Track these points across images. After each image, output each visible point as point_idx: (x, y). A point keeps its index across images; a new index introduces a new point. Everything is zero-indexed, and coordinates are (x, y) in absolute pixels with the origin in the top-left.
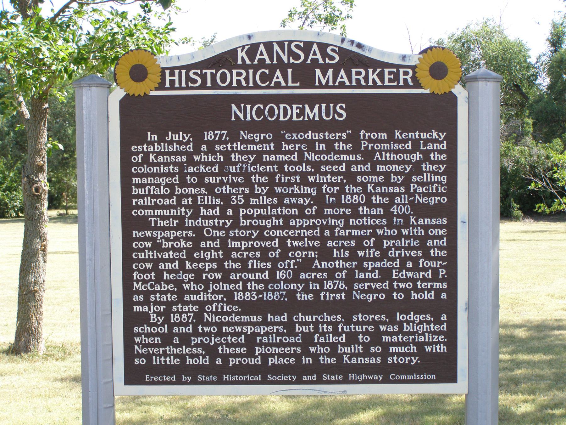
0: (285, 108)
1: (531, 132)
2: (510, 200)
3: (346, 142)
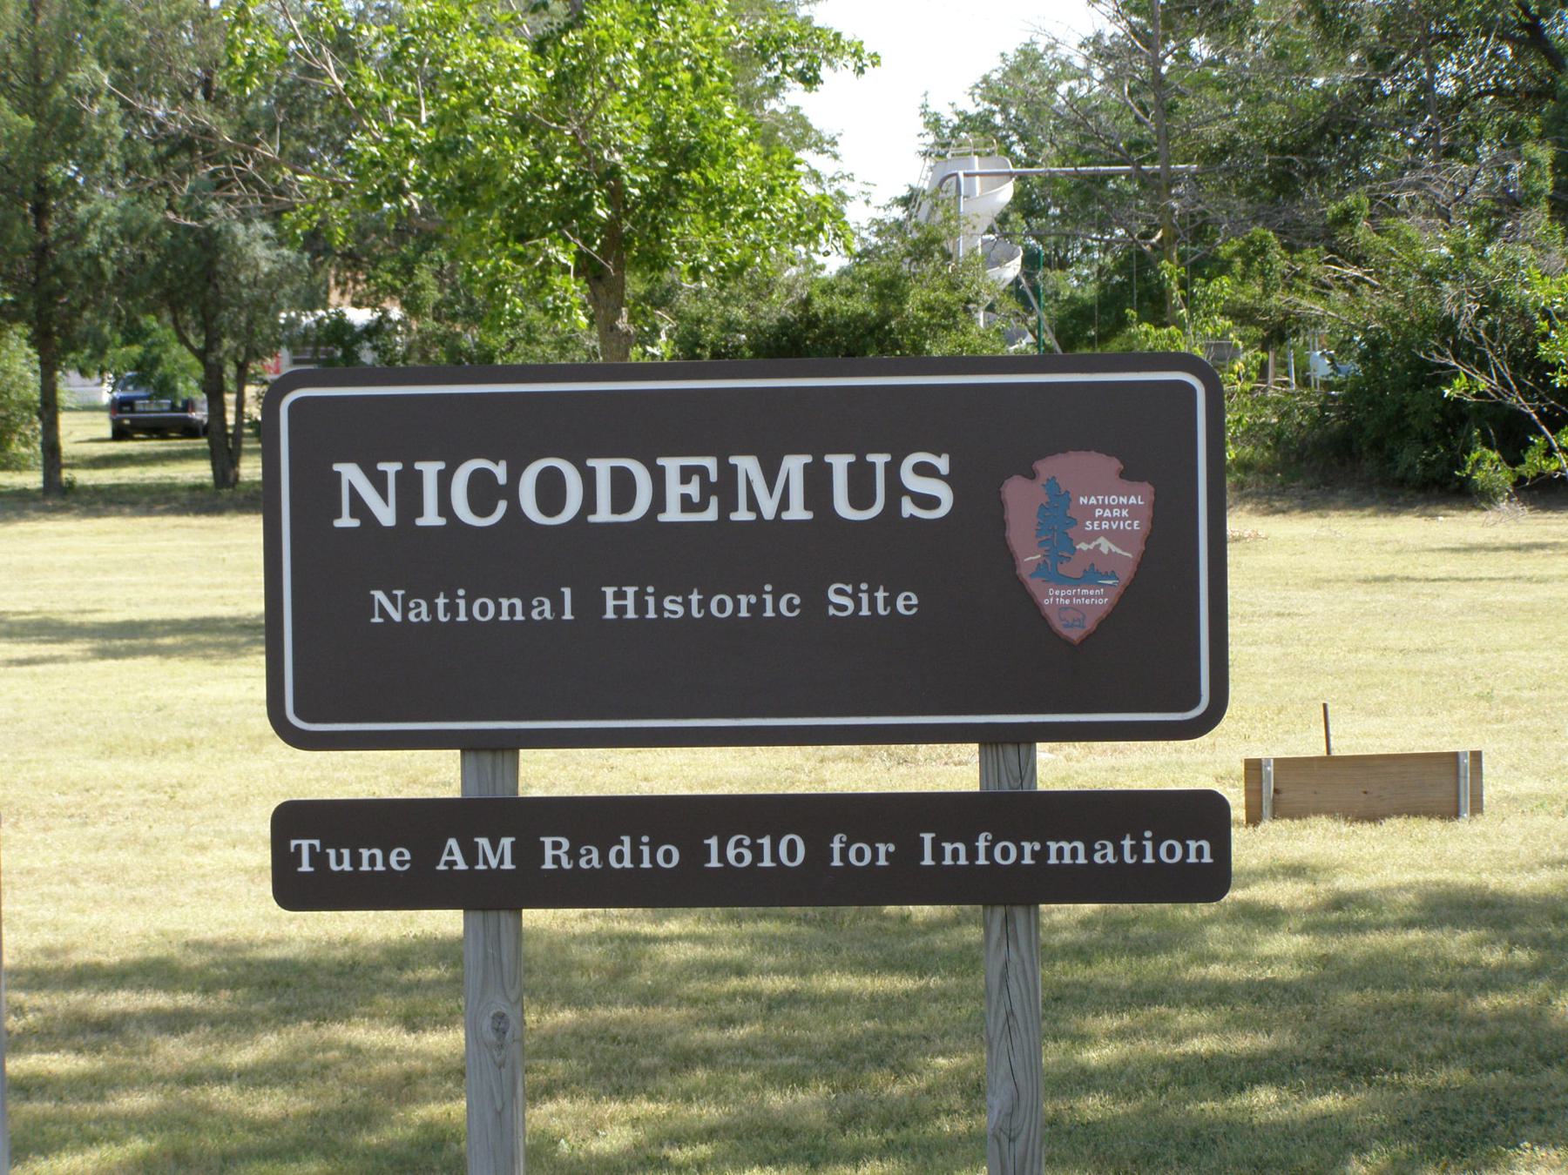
1: (1549, 192)
2: (1470, 433)
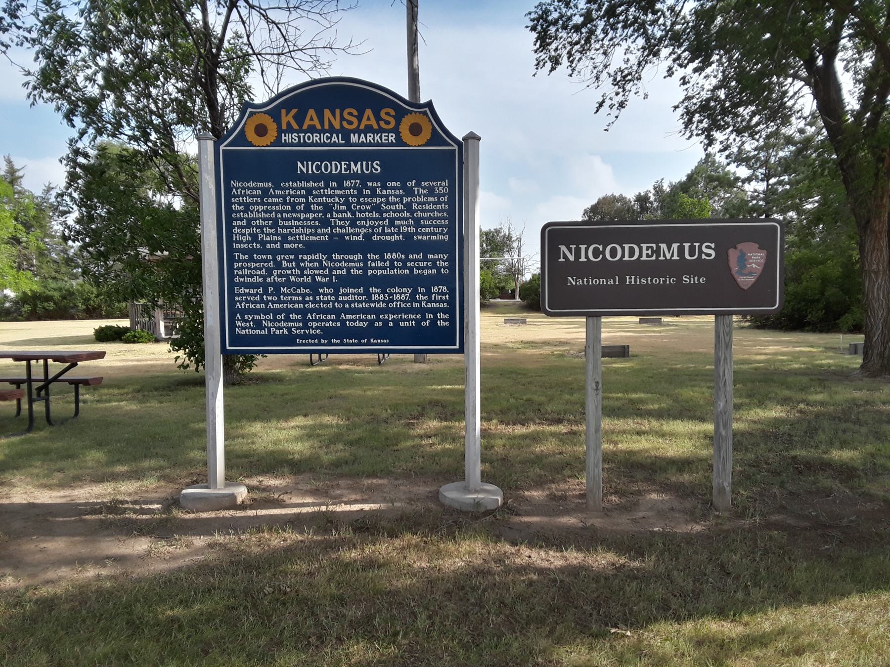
0: (336, 164)
3: (271, 228)
